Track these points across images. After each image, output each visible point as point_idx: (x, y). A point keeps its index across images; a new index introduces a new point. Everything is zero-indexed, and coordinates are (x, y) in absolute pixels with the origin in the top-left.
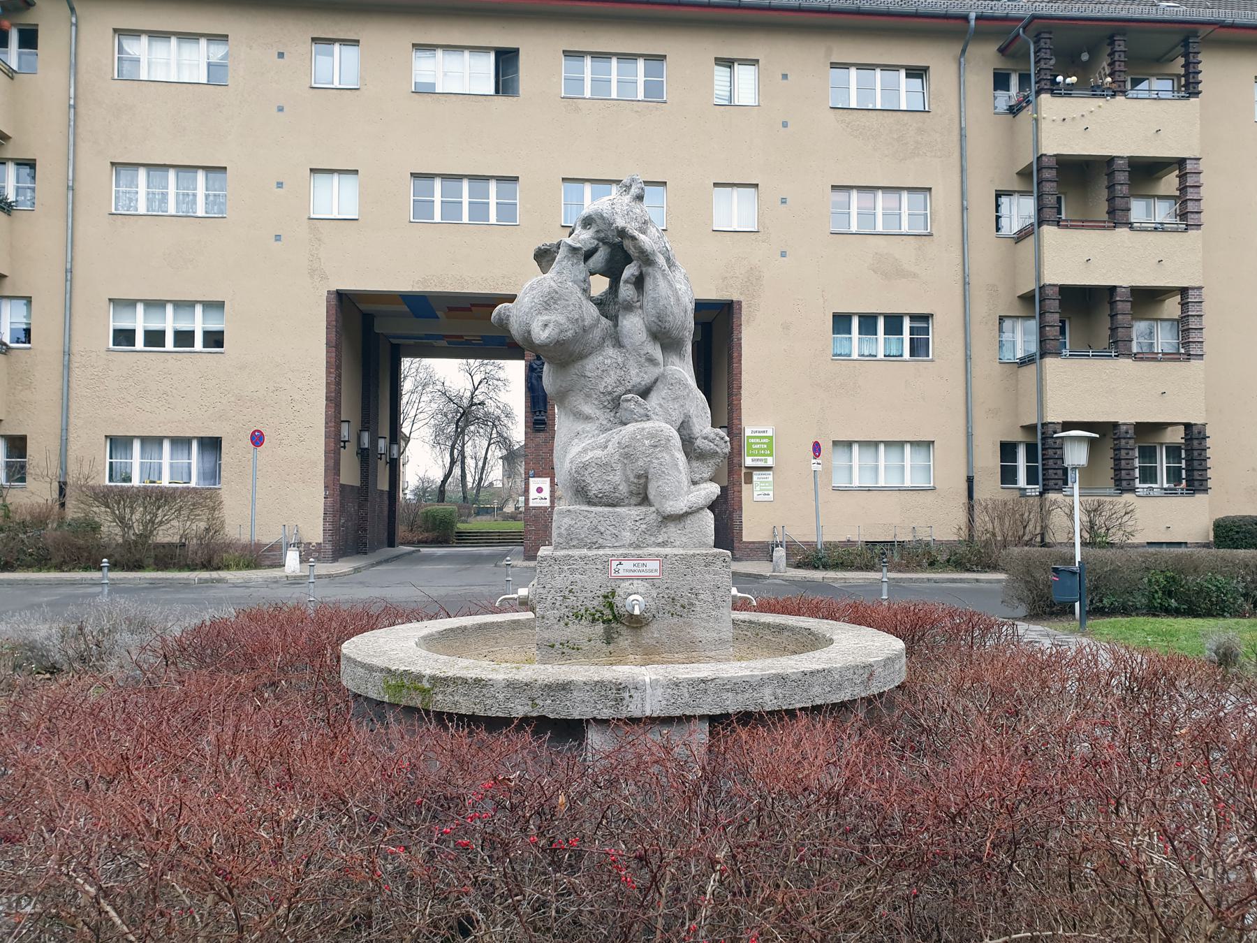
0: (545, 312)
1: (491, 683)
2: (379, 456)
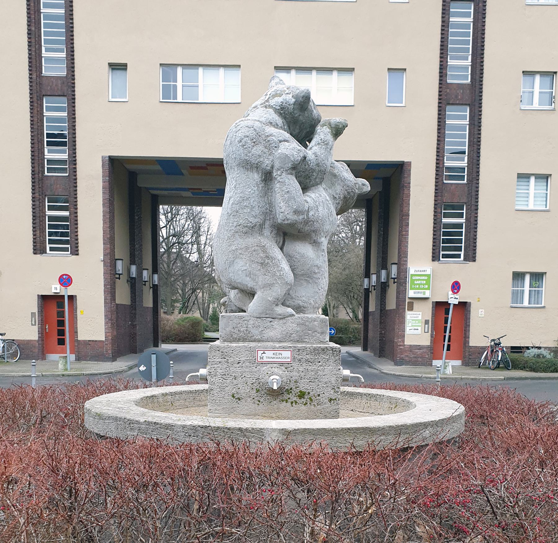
2: (144, 283)
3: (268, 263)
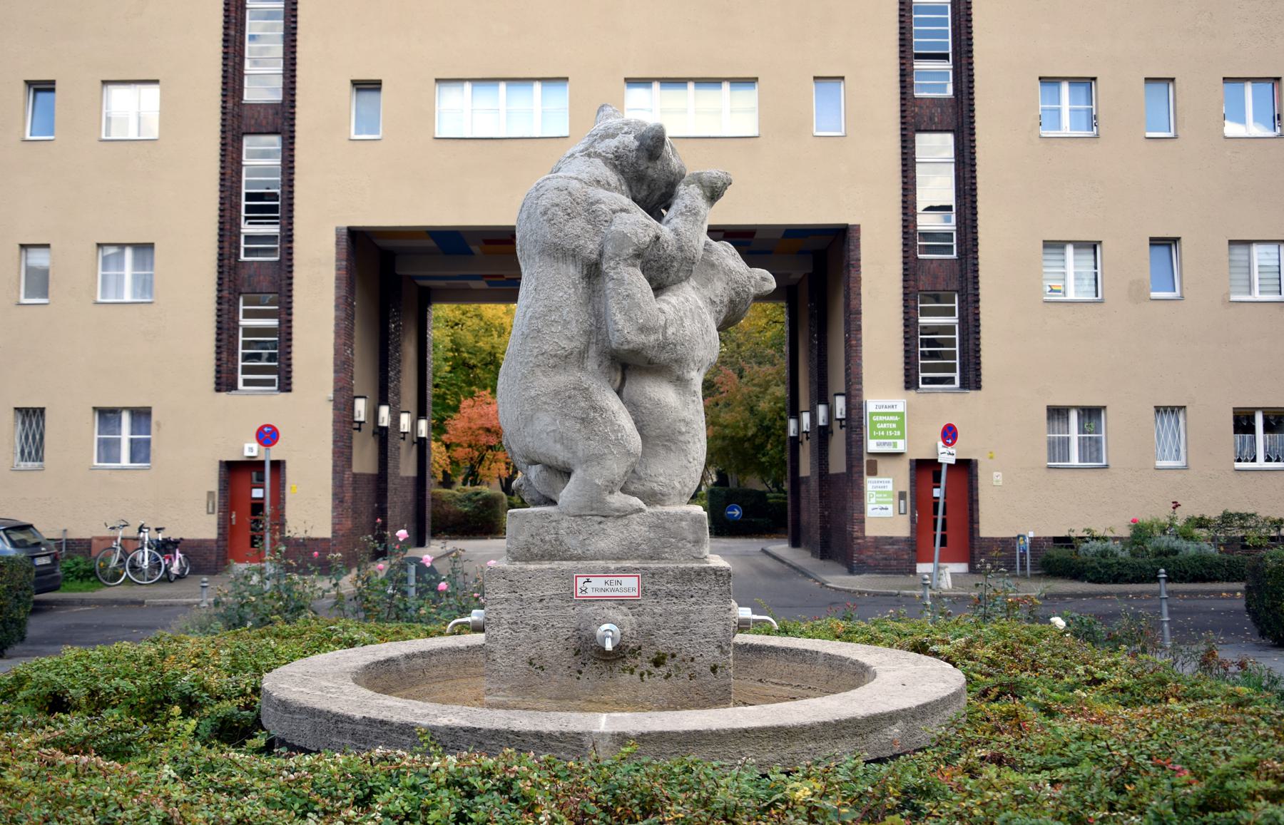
3: (594, 418)
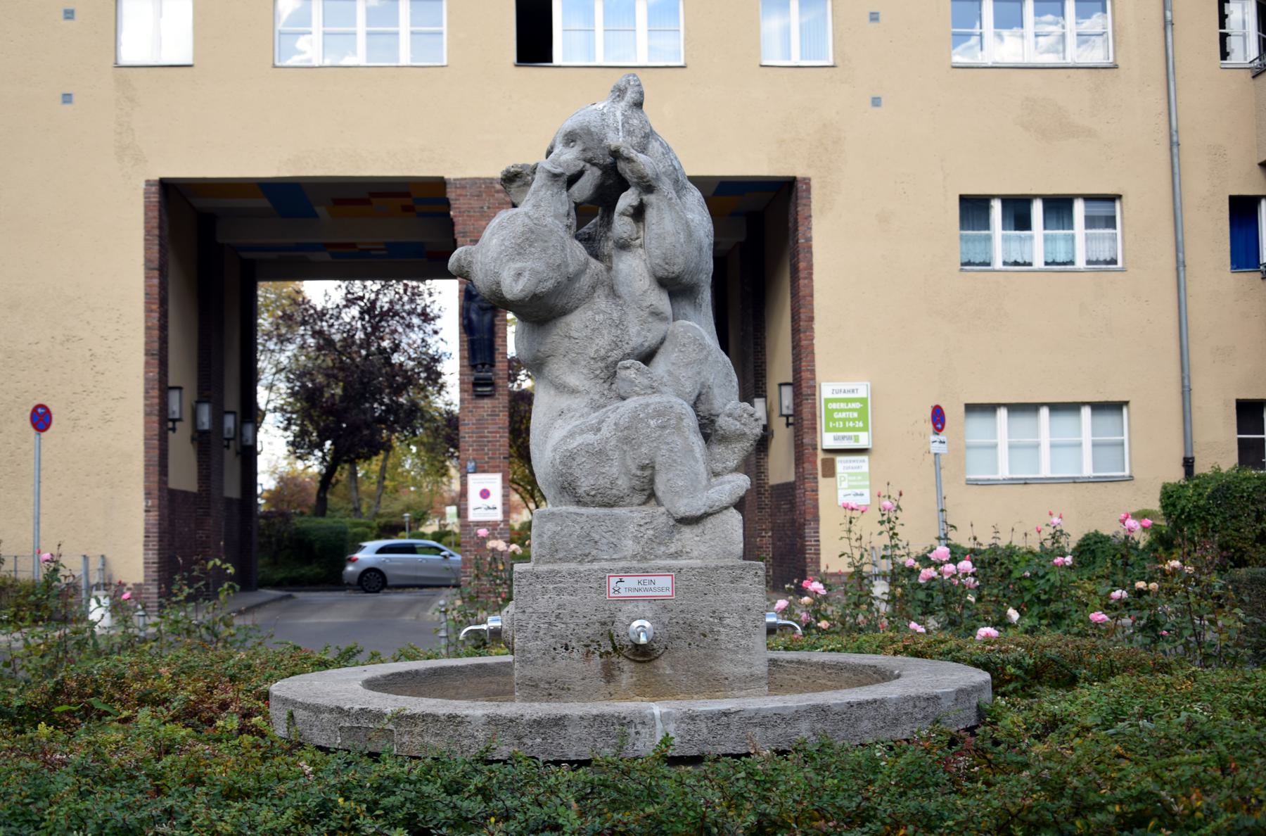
0: (517, 257)
1: (468, 719)
